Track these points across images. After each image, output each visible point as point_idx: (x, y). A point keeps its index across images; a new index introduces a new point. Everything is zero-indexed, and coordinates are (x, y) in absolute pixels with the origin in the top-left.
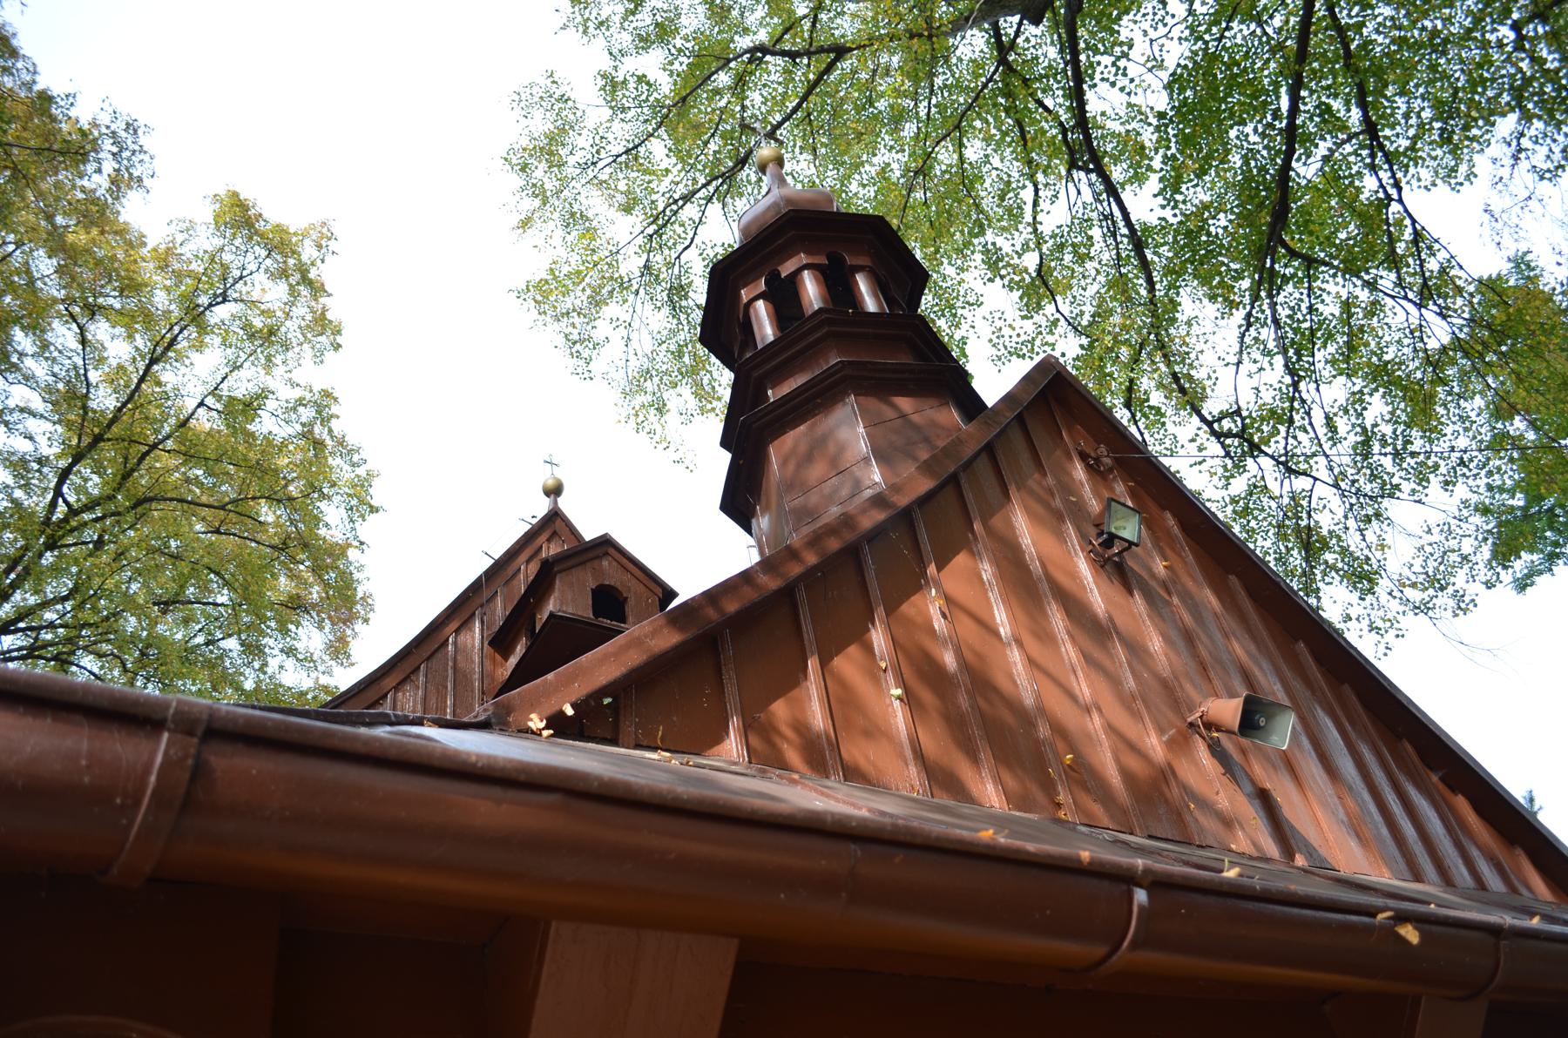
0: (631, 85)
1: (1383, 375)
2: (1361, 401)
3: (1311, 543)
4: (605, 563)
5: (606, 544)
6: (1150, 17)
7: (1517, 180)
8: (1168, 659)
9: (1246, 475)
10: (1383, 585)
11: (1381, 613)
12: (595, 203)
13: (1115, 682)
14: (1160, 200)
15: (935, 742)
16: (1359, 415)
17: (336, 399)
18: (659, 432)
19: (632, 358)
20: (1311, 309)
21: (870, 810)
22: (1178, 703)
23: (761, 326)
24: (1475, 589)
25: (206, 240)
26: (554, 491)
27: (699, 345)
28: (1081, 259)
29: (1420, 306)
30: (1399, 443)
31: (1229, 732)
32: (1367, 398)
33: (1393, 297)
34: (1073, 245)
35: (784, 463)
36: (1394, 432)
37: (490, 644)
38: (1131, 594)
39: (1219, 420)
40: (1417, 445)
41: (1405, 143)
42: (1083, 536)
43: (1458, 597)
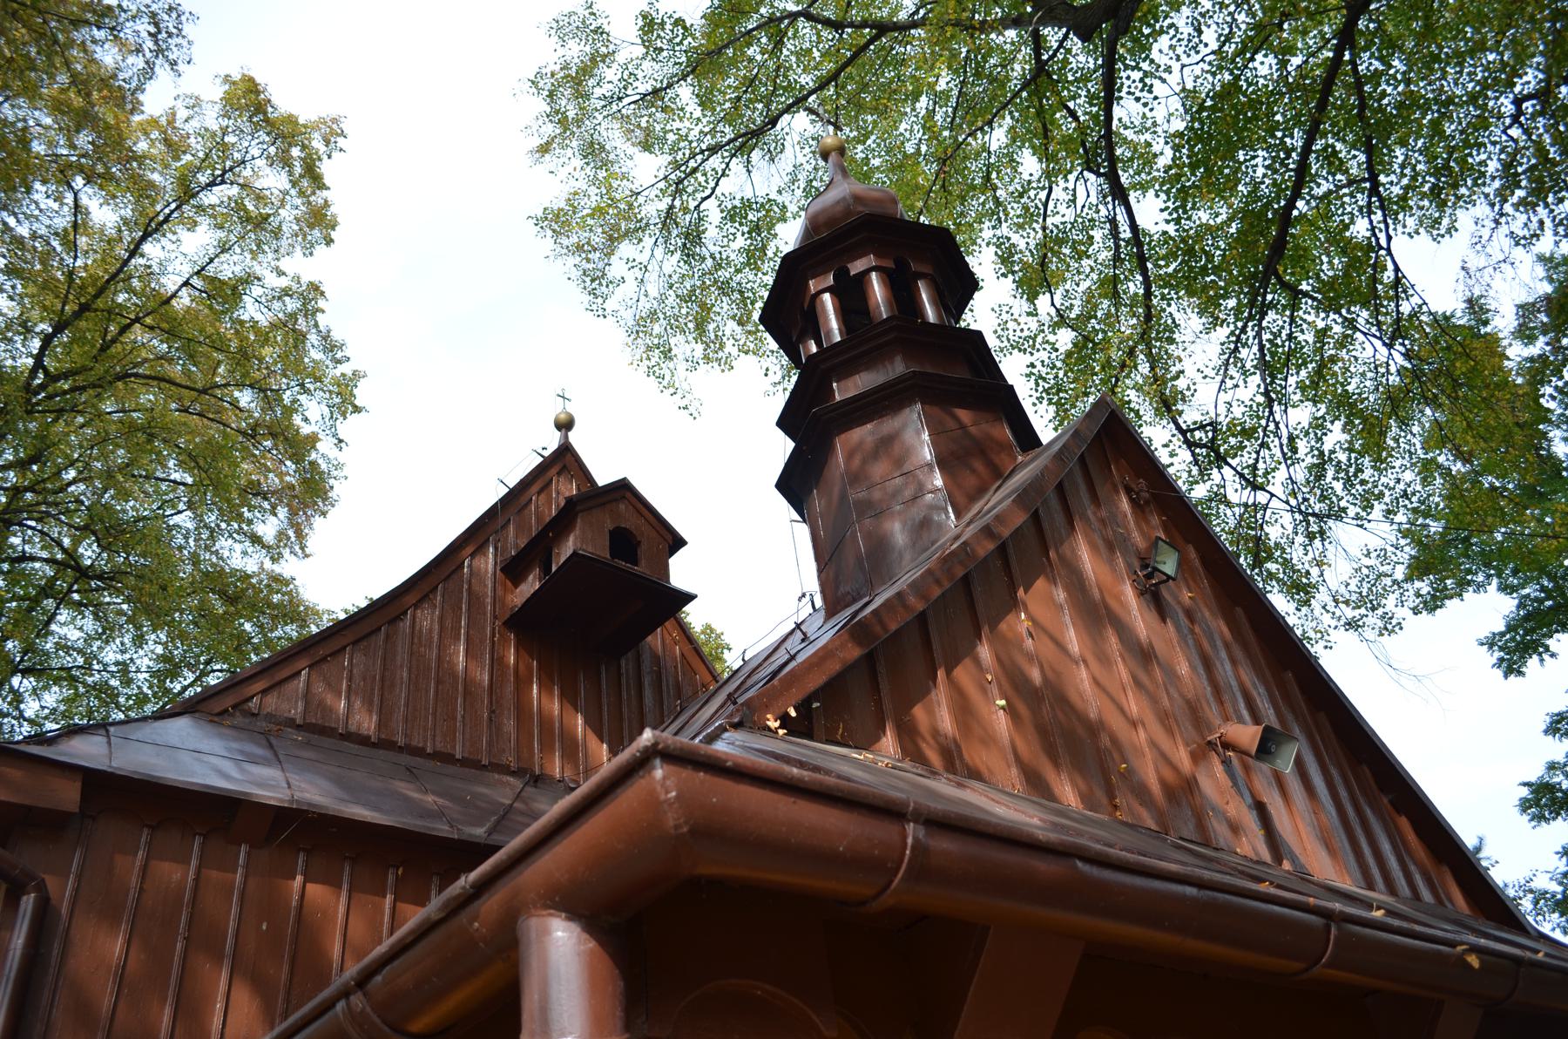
0: (668, 27)
1: (1345, 405)
2: (1322, 427)
3: (1261, 550)
4: (622, 507)
5: (623, 489)
7: (1495, 242)
10: (1322, 596)
11: (1314, 624)
12: (613, 136)
13: (1154, 700)
14: (1165, 215)
15: (1029, 748)
16: (1319, 440)
17: (322, 294)
18: (667, 378)
19: (642, 298)
20: (1290, 337)
22: (1198, 721)
23: (827, 320)
24: (1403, 613)
25: (211, 119)
26: (565, 425)
27: (761, 327)
28: (1081, 256)
29: (1390, 346)
30: (1352, 470)
32: (1329, 425)
35: (849, 457)
38: (1164, 621)
41: (1396, 190)
42: (1129, 565)
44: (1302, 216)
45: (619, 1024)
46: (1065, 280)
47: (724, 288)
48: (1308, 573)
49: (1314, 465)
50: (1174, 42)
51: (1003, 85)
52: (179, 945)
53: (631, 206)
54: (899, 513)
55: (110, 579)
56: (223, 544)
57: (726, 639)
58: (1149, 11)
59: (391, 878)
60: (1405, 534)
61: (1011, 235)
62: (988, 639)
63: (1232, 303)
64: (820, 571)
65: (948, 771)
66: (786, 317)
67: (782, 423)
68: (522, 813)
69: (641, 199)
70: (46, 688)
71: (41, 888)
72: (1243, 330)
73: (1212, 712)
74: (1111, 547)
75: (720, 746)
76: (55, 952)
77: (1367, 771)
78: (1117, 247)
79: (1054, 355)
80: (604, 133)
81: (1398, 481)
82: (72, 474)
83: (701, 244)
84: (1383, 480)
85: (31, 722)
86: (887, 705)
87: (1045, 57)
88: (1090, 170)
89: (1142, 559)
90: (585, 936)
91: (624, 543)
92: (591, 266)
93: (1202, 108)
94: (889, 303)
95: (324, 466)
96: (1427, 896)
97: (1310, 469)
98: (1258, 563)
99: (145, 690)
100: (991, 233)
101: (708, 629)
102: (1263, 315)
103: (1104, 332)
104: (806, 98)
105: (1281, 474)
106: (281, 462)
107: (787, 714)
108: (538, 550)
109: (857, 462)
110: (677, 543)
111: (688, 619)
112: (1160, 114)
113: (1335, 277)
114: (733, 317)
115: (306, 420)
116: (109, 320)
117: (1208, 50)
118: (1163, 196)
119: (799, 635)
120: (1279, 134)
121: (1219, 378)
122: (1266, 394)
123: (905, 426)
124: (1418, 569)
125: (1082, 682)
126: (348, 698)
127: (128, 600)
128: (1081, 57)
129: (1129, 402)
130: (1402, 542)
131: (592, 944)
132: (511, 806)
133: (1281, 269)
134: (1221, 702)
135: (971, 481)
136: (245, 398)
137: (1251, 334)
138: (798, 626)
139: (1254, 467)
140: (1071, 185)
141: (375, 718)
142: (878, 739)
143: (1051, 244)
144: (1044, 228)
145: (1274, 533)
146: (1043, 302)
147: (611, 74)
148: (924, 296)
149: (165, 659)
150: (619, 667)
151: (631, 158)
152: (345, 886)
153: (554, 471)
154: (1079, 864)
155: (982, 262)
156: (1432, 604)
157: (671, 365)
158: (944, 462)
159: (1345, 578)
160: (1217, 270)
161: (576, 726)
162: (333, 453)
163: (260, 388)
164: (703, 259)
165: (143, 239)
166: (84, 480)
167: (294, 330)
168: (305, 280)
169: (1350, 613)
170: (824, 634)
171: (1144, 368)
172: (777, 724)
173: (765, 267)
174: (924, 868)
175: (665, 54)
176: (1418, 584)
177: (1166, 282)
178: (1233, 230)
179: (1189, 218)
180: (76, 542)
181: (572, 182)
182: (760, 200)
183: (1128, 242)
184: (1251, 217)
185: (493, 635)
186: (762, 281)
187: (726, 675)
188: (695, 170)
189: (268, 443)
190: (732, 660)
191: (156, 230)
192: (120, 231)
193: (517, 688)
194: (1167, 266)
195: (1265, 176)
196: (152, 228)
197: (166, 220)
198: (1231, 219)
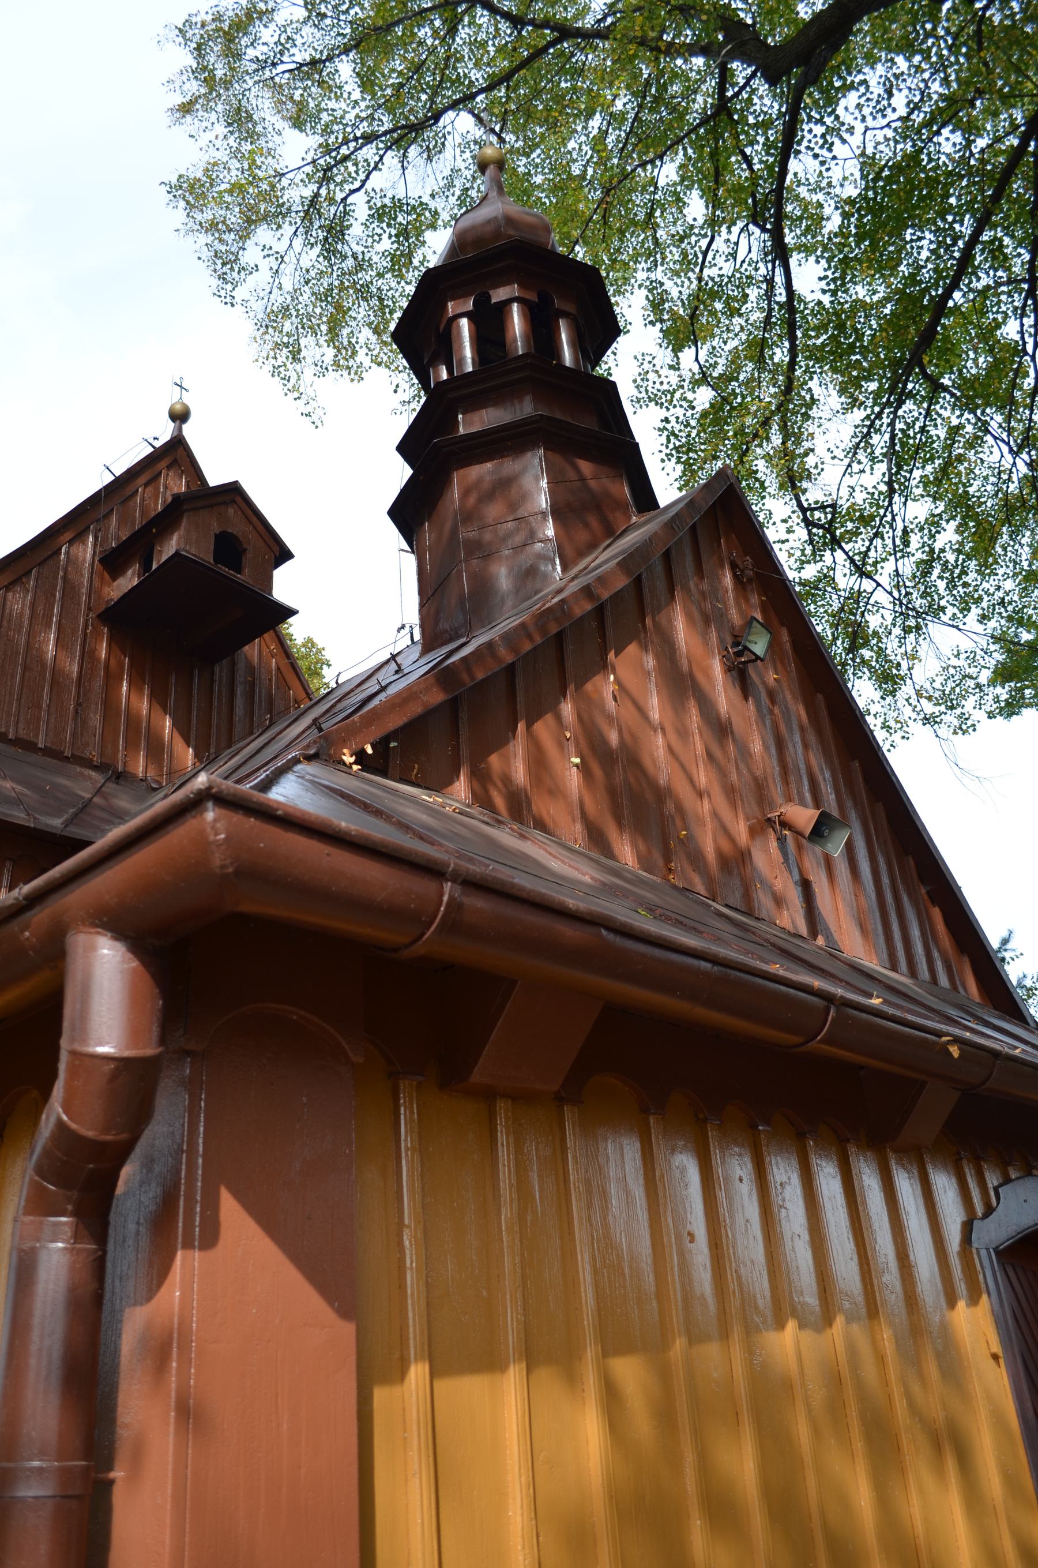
1: (962, 505)
2: (937, 524)
3: (858, 636)
4: (231, 511)
5: (233, 492)
6: (873, 104)
8: (763, 761)
9: (821, 564)
10: (907, 690)
12: (263, 106)
13: (722, 773)
14: (823, 284)
15: (597, 807)
16: (932, 536)
18: (293, 381)
19: (275, 290)
20: (923, 430)
21: (592, 878)
23: (461, 347)
26: (180, 416)
28: (733, 312)
29: (1015, 454)
30: (957, 571)
31: (798, 833)
32: (944, 523)
33: (995, 438)
34: (729, 297)
35: (465, 494)
36: (957, 561)
37: (100, 561)
38: (746, 699)
39: (813, 510)
40: (971, 577)
42: (721, 640)
43: (963, 718)
44: (957, 307)
46: (713, 336)
47: (363, 292)
48: (899, 664)
49: (923, 561)
50: (862, 101)
51: (682, 116)
53: (273, 187)
57: (327, 655)
58: (843, 62)
60: (996, 639)
61: (665, 280)
62: (572, 698)
63: (873, 386)
66: (418, 338)
67: (401, 448)
68: (102, 809)
69: (285, 182)
72: (879, 416)
73: (776, 790)
74: (707, 621)
77: (912, 862)
78: (770, 310)
79: (689, 413)
80: (253, 101)
81: (998, 588)
83: (343, 241)
84: (985, 585)
86: (464, 751)
87: (729, 94)
88: (756, 224)
89: (736, 636)
90: (129, 955)
91: (229, 548)
92: (223, 248)
93: (878, 177)
94: (526, 338)
96: (944, 981)
97: (917, 564)
98: (852, 649)
100: (645, 275)
101: (310, 643)
102: (900, 403)
103: (744, 397)
104: (473, 96)
105: (889, 566)
107: (363, 751)
108: (138, 546)
109: (472, 500)
110: (284, 555)
112: (836, 174)
113: (976, 377)
114: (370, 325)
117: (895, 116)
118: (823, 263)
119: (393, 667)
120: (950, 218)
121: (847, 461)
122: (890, 484)
123: (524, 470)
124: (1002, 675)
125: (657, 749)
128: (765, 102)
129: (756, 472)
130: (992, 647)
131: (135, 963)
132: (90, 800)
133: (926, 359)
134: (786, 782)
135: (582, 536)
137: (886, 421)
138: (394, 657)
139: (865, 554)
140: (733, 238)
142: (451, 783)
143: (704, 296)
144: (700, 279)
145: (874, 622)
146: (687, 356)
147: (268, 34)
148: (564, 336)
150: (213, 673)
151: (279, 133)
153: (163, 464)
154: (604, 932)
155: (631, 307)
156: (1011, 708)
157: (298, 367)
159: (932, 674)
160: (864, 351)
161: (164, 727)
164: (344, 257)
169: (929, 708)
170: (416, 667)
171: (777, 440)
172: (352, 759)
174: (455, 922)
175: (328, 21)
176: (999, 690)
177: (817, 355)
178: (887, 311)
179: (846, 292)
181: (212, 152)
182: (412, 202)
183: (781, 306)
184: (906, 300)
185: (86, 627)
186: (402, 291)
187: (323, 692)
188: (346, 158)
190: (329, 675)
194: (817, 337)
195: (928, 259)
198: (887, 299)
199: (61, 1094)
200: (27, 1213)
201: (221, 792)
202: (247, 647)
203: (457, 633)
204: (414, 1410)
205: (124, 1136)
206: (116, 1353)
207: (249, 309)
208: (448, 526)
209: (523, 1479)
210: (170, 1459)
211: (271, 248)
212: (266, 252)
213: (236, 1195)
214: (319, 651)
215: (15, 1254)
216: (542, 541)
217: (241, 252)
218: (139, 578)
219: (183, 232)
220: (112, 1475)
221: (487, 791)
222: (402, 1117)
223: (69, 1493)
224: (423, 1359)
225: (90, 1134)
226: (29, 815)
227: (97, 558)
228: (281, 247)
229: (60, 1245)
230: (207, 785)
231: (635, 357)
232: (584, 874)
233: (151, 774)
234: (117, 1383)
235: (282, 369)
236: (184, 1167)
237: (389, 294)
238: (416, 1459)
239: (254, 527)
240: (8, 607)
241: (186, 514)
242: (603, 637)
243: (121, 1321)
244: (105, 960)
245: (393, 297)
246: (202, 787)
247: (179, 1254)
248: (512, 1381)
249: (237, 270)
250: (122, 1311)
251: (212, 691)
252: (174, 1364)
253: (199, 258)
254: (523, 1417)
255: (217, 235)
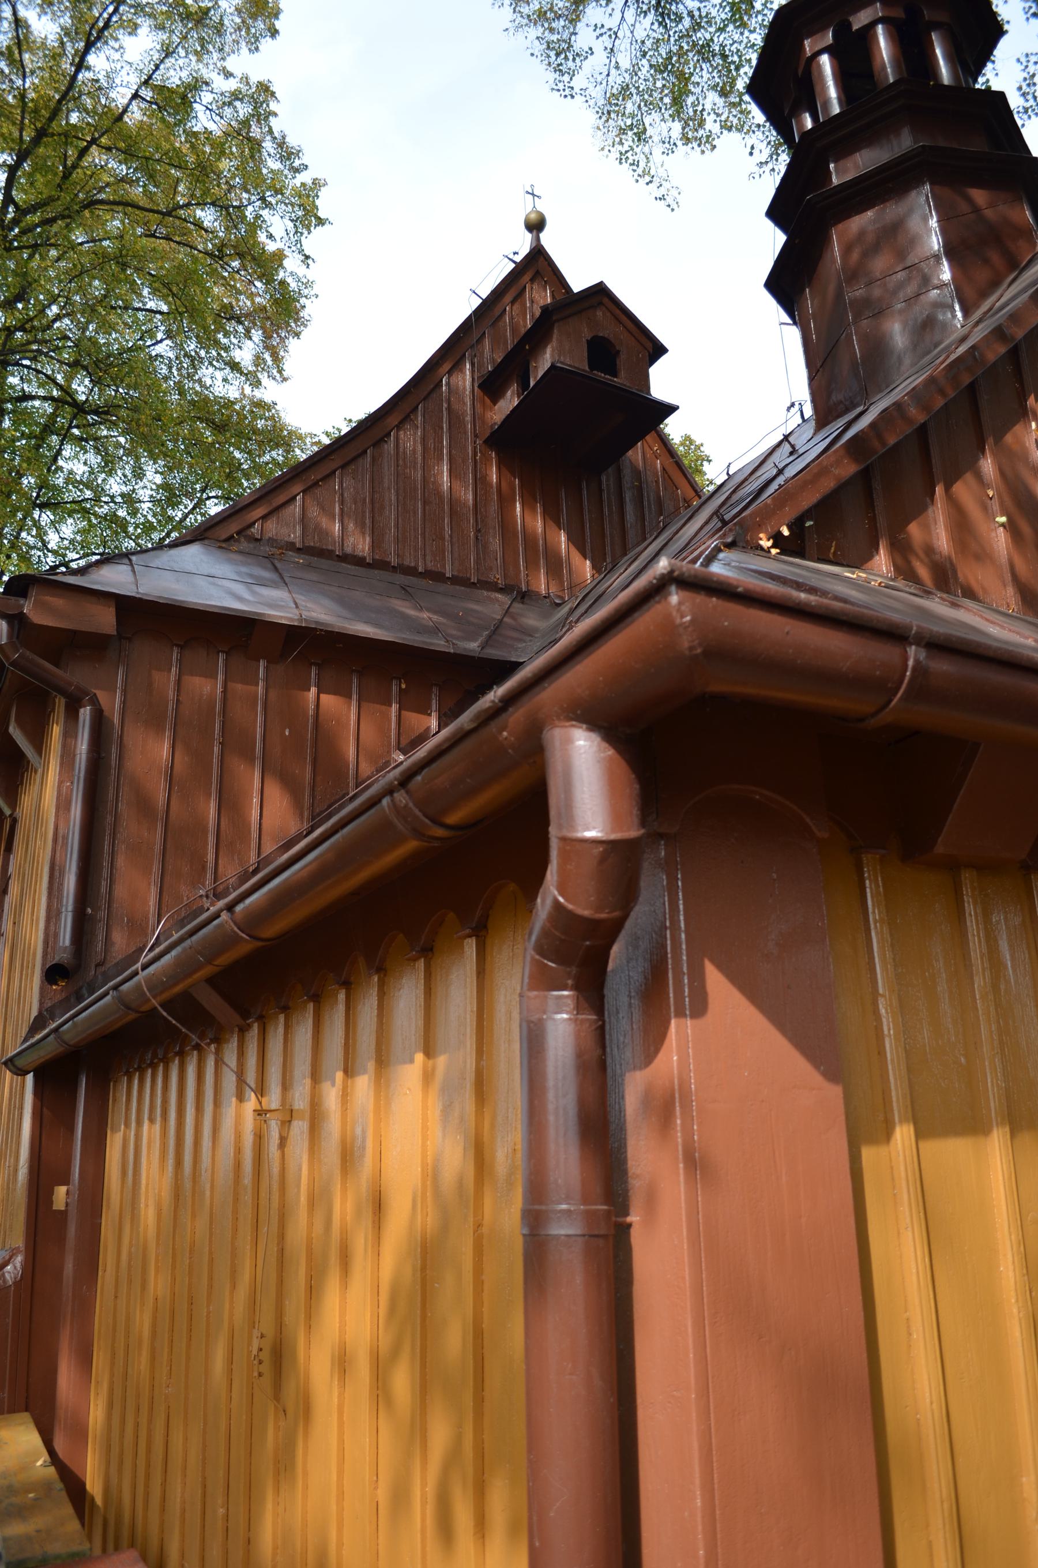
4: (599, 313)
5: (600, 293)
17: (273, 94)
18: (642, 164)
19: (613, 71)
26: (536, 225)
27: (747, 98)
35: (847, 251)
37: (479, 387)
45: (636, 820)
47: (704, 51)
52: (216, 749)
54: (901, 312)
55: (105, 412)
56: (205, 372)
57: (706, 450)
59: (395, 689)
62: (993, 453)
64: (811, 379)
65: (940, 588)
70: (62, 520)
71: (94, 701)
75: (716, 568)
76: (113, 756)
82: (55, 309)
85: (55, 553)
86: (882, 522)
90: (605, 745)
91: (602, 353)
94: (896, 62)
95: (293, 285)
99: (150, 518)
101: (688, 440)
106: (251, 282)
107: (780, 533)
109: (855, 256)
110: (658, 350)
111: (667, 431)
114: (714, 87)
115: (271, 237)
116: (66, 144)
119: (786, 448)
123: (911, 211)
126: (342, 521)
127: (123, 433)
131: (611, 752)
132: (501, 621)
135: (982, 275)
136: (207, 216)
138: (786, 438)
141: (368, 539)
142: (870, 557)
149: (165, 486)
152: (355, 697)
153: (526, 278)
157: (646, 150)
158: (954, 250)
161: (559, 542)
162: (301, 270)
163: (222, 206)
164: (679, 19)
165: (89, 46)
166: (68, 315)
167: (249, 139)
168: (254, 80)
172: (770, 543)
173: (753, 23)
174: (923, 687)
180: (69, 379)
185: (475, 454)
186: (748, 43)
187: (711, 488)
189: (236, 264)
191: (98, 38)
192: (62, 43)
193: (501, 507)
196: (93, 36)
197: (107, 25)
199: (555, 878)
200: (531, 988)
201: (682, 574)
202: (630, 452)
203: (852, 402)
204: (902, 1168)
205: (616, 914)
206: (621, 1111)
207: (588, 97)
208: (832, 288)
209: (1013, 1237)
210: (683, 1205)
211: (603, 26)
212: (598, 32)
213: (719, 967)
214: (698, 447)
215: (525, 1025)
216: (937, 288)
217: (573, 38)
218: (518, 397)
219: (512, 31)
220: (629, 1219)
221: (909, 562)
222: (868, 890)
223: (596, 1233)
224: (907, 1121)
225: (586, 913)
226: (448, 641)
227: (476, 385)
228: (612, 23)
229: (565, 1016)
230: (669, 569)
231: (1018, 60)
232: (1027, 638)
233: (553, 590)
234: (625, 1139)
235: (629, 154)
236: (669, 942)
237: (733, 48)
238: (907, 1213)
239: (625, 327)
240: (401, 445)
241: (556, 325)
242: (1021, 381)
243: (623, 1084)
244: (582, 751)
245: (738, 50)
246: (665, 571)
247: (673, 1022)
248: (996, 1145)
249: (571, 58)
250: (622, 1075)
251: (601, 501)
252: (679, 1122)
253: (532, 55)
254: (1010, 1178)
255: (546, 25)
